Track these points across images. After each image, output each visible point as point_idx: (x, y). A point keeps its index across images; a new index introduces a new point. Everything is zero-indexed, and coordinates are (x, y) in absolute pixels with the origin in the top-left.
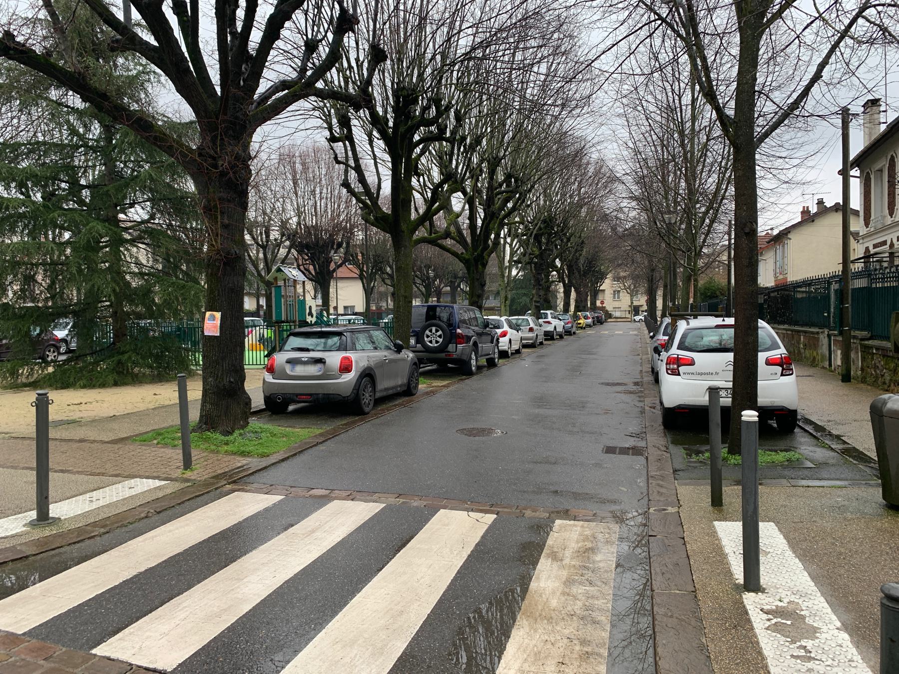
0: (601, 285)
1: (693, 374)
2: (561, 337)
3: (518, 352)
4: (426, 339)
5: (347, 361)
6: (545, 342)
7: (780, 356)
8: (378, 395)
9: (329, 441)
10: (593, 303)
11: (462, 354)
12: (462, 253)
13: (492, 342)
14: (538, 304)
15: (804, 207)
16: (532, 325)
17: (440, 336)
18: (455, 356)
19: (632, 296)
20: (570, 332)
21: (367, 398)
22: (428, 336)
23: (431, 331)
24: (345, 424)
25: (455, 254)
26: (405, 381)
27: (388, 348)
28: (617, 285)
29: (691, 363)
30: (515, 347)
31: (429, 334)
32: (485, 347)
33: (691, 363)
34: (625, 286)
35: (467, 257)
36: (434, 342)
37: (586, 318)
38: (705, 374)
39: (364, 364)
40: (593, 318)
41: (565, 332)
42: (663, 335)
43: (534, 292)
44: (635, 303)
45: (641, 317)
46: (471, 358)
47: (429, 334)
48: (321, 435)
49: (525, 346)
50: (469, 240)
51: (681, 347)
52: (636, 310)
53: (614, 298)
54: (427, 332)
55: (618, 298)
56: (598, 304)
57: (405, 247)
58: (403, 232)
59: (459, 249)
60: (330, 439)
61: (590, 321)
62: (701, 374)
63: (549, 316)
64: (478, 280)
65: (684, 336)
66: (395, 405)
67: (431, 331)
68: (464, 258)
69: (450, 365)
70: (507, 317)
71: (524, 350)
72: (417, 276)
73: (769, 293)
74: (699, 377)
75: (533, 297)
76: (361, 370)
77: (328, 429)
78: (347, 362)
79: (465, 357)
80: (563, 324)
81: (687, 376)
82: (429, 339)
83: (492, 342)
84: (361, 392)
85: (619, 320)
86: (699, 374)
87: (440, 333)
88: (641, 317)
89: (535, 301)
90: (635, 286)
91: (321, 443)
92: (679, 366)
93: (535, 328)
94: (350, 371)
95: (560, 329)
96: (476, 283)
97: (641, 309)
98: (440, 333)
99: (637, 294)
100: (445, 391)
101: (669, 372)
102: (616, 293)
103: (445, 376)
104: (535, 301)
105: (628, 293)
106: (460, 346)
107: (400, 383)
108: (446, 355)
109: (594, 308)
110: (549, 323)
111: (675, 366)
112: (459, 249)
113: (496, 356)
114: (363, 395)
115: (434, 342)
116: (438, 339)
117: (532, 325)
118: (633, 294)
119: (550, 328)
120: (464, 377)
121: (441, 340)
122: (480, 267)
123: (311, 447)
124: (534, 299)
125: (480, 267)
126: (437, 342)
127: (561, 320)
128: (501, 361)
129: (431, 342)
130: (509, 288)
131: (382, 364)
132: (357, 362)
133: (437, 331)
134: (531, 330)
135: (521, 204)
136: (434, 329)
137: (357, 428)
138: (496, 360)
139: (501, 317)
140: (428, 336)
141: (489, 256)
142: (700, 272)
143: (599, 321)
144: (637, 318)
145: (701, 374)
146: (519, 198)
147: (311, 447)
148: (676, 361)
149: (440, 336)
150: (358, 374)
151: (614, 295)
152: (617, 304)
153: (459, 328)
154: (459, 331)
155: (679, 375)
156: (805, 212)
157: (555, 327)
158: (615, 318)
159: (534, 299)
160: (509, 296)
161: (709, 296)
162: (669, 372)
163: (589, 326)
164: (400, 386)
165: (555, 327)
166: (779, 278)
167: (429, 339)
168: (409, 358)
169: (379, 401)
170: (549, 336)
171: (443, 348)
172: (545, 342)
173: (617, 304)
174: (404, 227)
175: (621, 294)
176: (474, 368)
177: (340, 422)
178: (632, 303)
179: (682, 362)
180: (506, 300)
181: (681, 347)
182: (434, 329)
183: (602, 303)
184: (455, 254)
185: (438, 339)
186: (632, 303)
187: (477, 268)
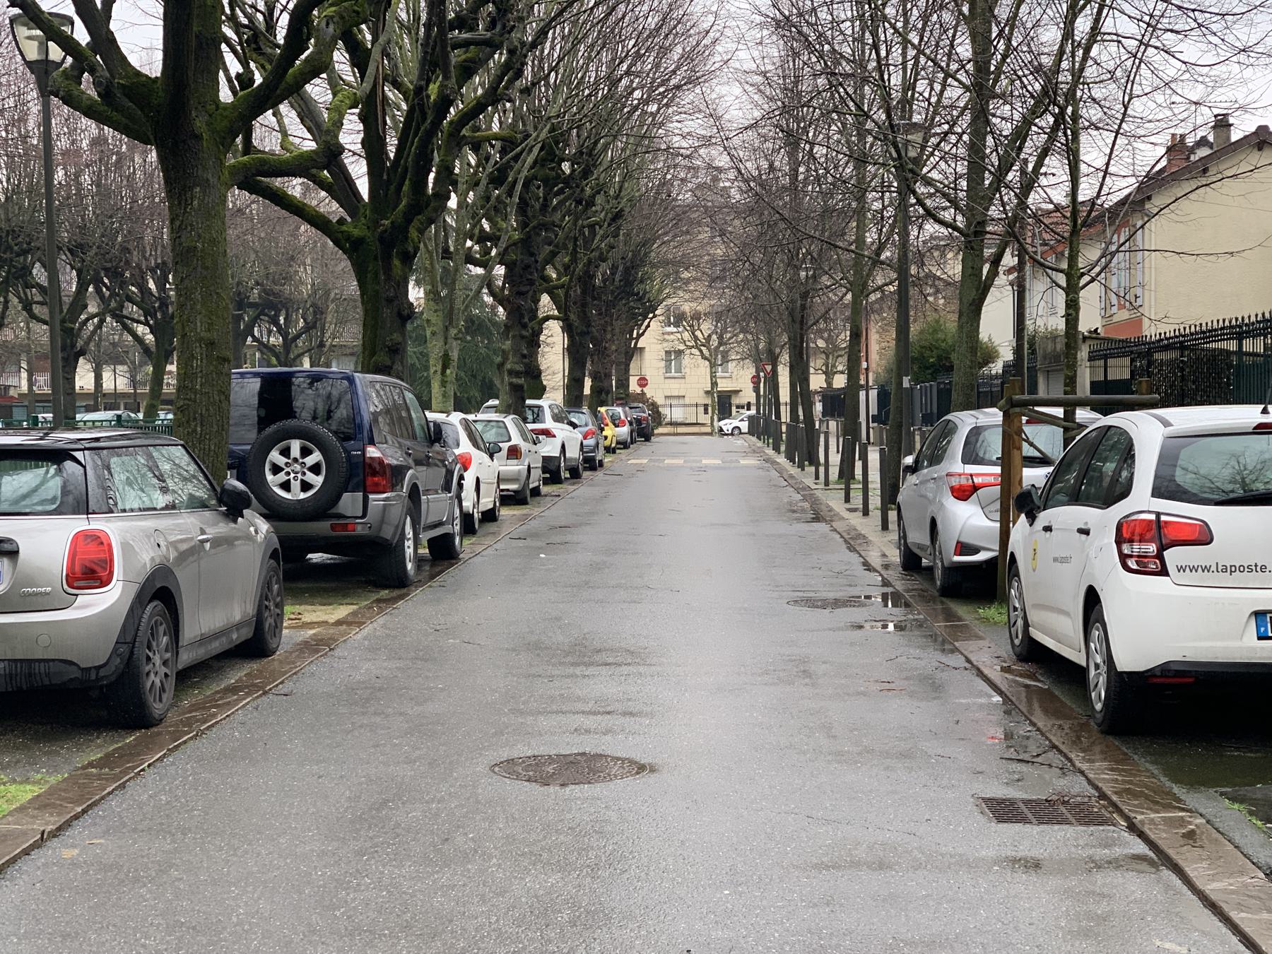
0: (639, 336)
1: (1206, 569)
2: (575, 474)
3: (490, 516)
4: (270, 477)
5: (93, 547)
6: (545, 489)
7: (1153, 517)
8: (186, 658)
9: (77, 828)
10: (624, 383)
11: (382, 521)
12: (341, 221)
13: (447, 488)
14: (521, 381)
15: (1173, 135)
16: (516, 439)
17: (315, 469)
18: (360, 530)
19: (713, 366)
20: (593, 459)
21: (156, 674)
22: (276, 469)
23: (286, 452)
24: (99, 764)
25: (319, 222)
26: (251, 610)
27: (197, 504)
28: (678, 336)
29: (1203, 537)
30: (487, 502)
31: (281, 461)
32: (436, 505)
33: (1203, 537)
34: (696, 338)
35: (356, 232)
36: (296, 485)
37: (617, 422)
38: (1241, 569)
39: (147, 558)
40: (631, 423)
41: (586, 460)
42: (966, 460)
43: (508, 344)
44: (723, 385)
45: (736, 423)
46: (403, 537)
47: (281, 461)
48: (40, 804)
49: (508, 499)
50: (363, 187)
51: (1164, 488)
52: (723, 404)
53: (668, 369)
54: (275, 456)
55: (679, 370)
56: (634, 387)
57: (206, 185)
58: (198, 138)
59: (330, 208)
60: (76, 817)
61: (624, 431)
62: (1232, 569)
63: (548, 414)
64: (390, 301)
65: (1168, 459)
66: (233, 690)
67: (286, 452)
68: (348, 237)
69: (315, 557)
70: (463, 416)
71: (505, 512)
72: (130, 299)
73: (1149, 353)
74: (1226, 579)
75: (505, 359)
76: (142, 579)
77: (53, 780)
78: (93, 554)
79: (387, 533)
80: (580, 437)
81: (1187, 577)
82: (282, 477)
83: (447, 488)
84: (141, 651)
85: (681, 430)
86: (1225, 570)
87: (316, 457)
88: (736, 423)
89: (511, 372)
90: (721, 337)
91: (55, 834)
92: (1162, 548)
93: (524, 446)
94: (104, 582)
95: (573, 453)
96: (387, 312)
97: (736, 401)
98: (316, 457)
99: (726, 360)
100: (358, 636)
101: (1132, 564)
102: (673, 356)
103: (326, 591)
104: (511, 372)
105: (704, 358)
106: (376, 499)
107: (237, 616)
108: (333, 527)
109: (625, 398)
110: (547, 433)
111: (1152, 548)
112: (330, 208)
113: (457, 528)
114: (149, 659)
115: (296, 485)
116: (310, 477)
117: (516, 439)
118: (717, 358)
119: (550, 448)
120: (384, 593)
121: (317, 480)
122: (396, 262)
123: (26, 852)
124: (508, 366)
125: (396, 262)
126: (306, 486)
127: (574, 426)
128: (466, 542)
129: (286, 486)
130: (453, 332)
131: (192, 552)
132: (126, 546)
133: (305, 452)
134: (514, 453)
135: (511, 82)
136: (296, 446)
137: (150, 775)
138: (457, 540)
139: (448, 413)
140: (276, 469)
141: (421, 232)
142: (1086, 279)
143: (643, 432)
144: (727, 425)
145: (1232, 569)
146: (506, 67)
147: (26, 852)
148: (1154, 532)
149: (315, 469)
150: (133, 590)
151: (668, 361)
152: (674, 387)
153: (372, 442)
154: (372, 452)
155: (1164, 572)
156: (1177, 148)
157: (563, 446)
158: (671, 424)
159: (508, 366)
160: (455, 355)
161: (933, 365)
162: (1132, 564)
163: (624, 445)
164: (238, 626)
165: (563, 446)
166: (1115, 319)
167: (282, 477)
168: (260, 537)
169: (187, 677)
170: (552, 471)
171: (323, 507)
172: (545, 489)
173: (674, 387)
174: (200, 123)
175: (686, 360)
176: (409, 566)
177: (95, 750)
178: (714, 384)
179: (1170, 535)
180: (445, 367)
181: (1164, 488)
182: (296, 446)
183: (643, 382)
184: (319, 222)
185: (310, 477)
186: (714, 384)
187: (388, 269)
